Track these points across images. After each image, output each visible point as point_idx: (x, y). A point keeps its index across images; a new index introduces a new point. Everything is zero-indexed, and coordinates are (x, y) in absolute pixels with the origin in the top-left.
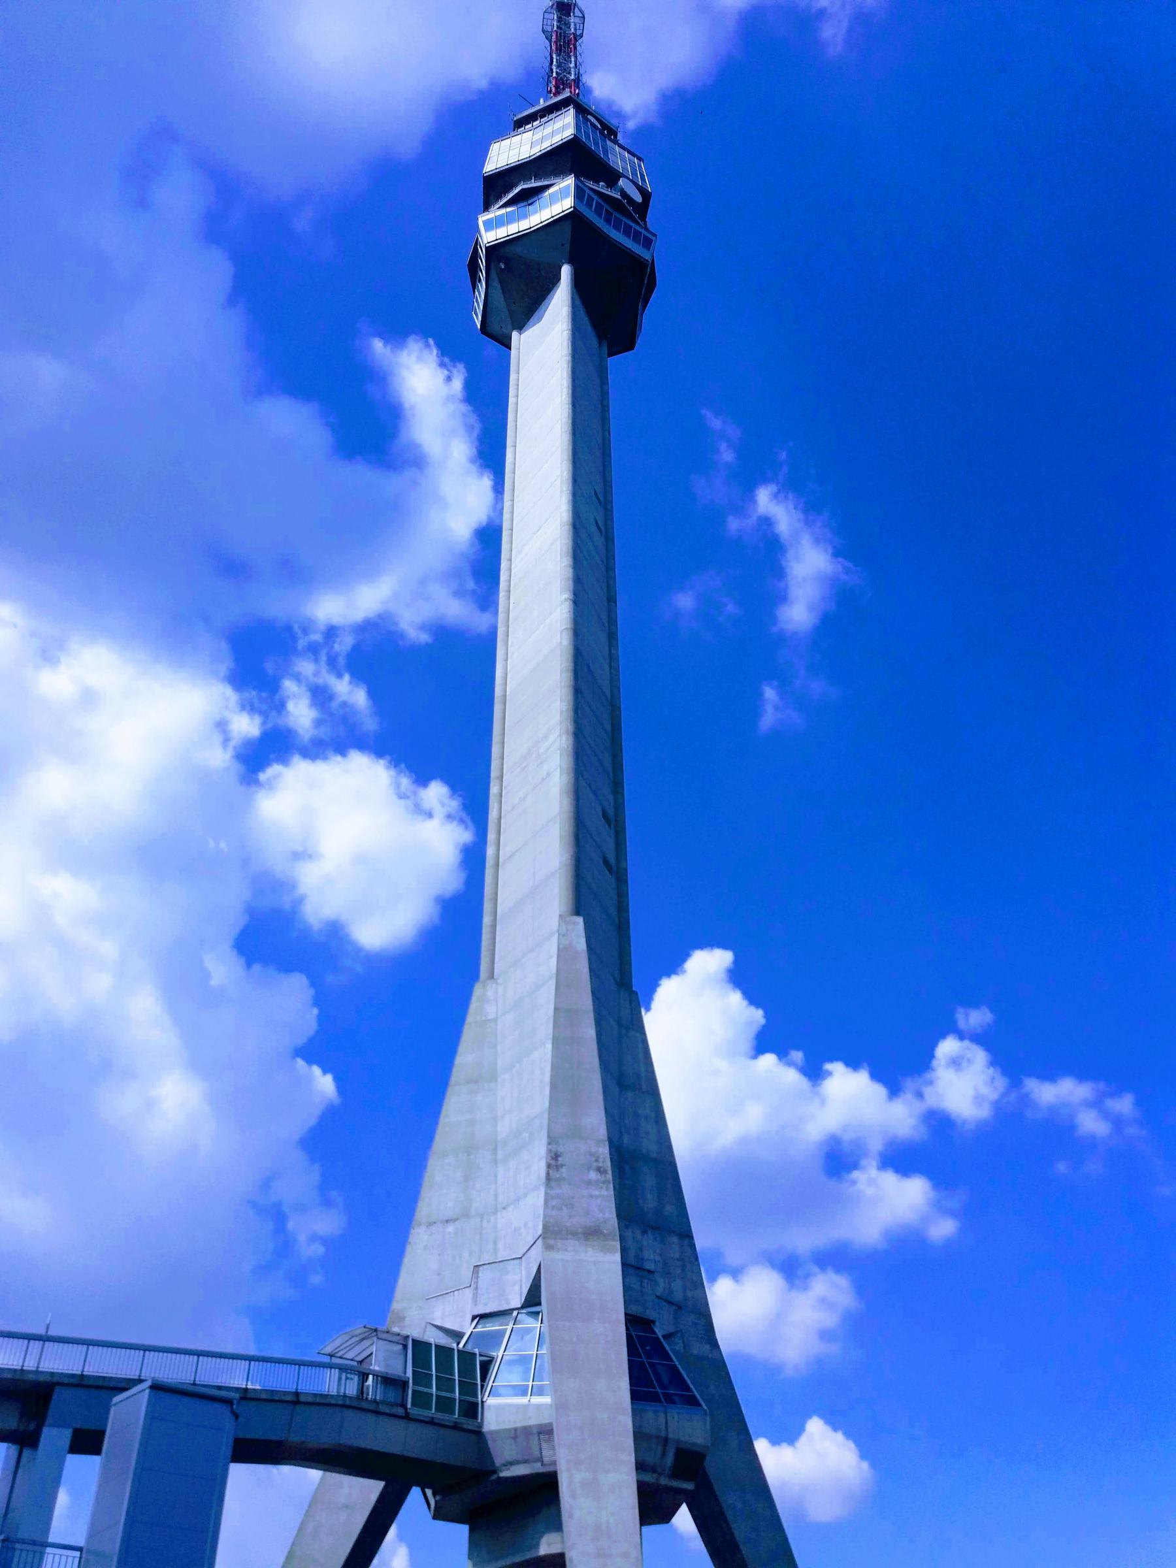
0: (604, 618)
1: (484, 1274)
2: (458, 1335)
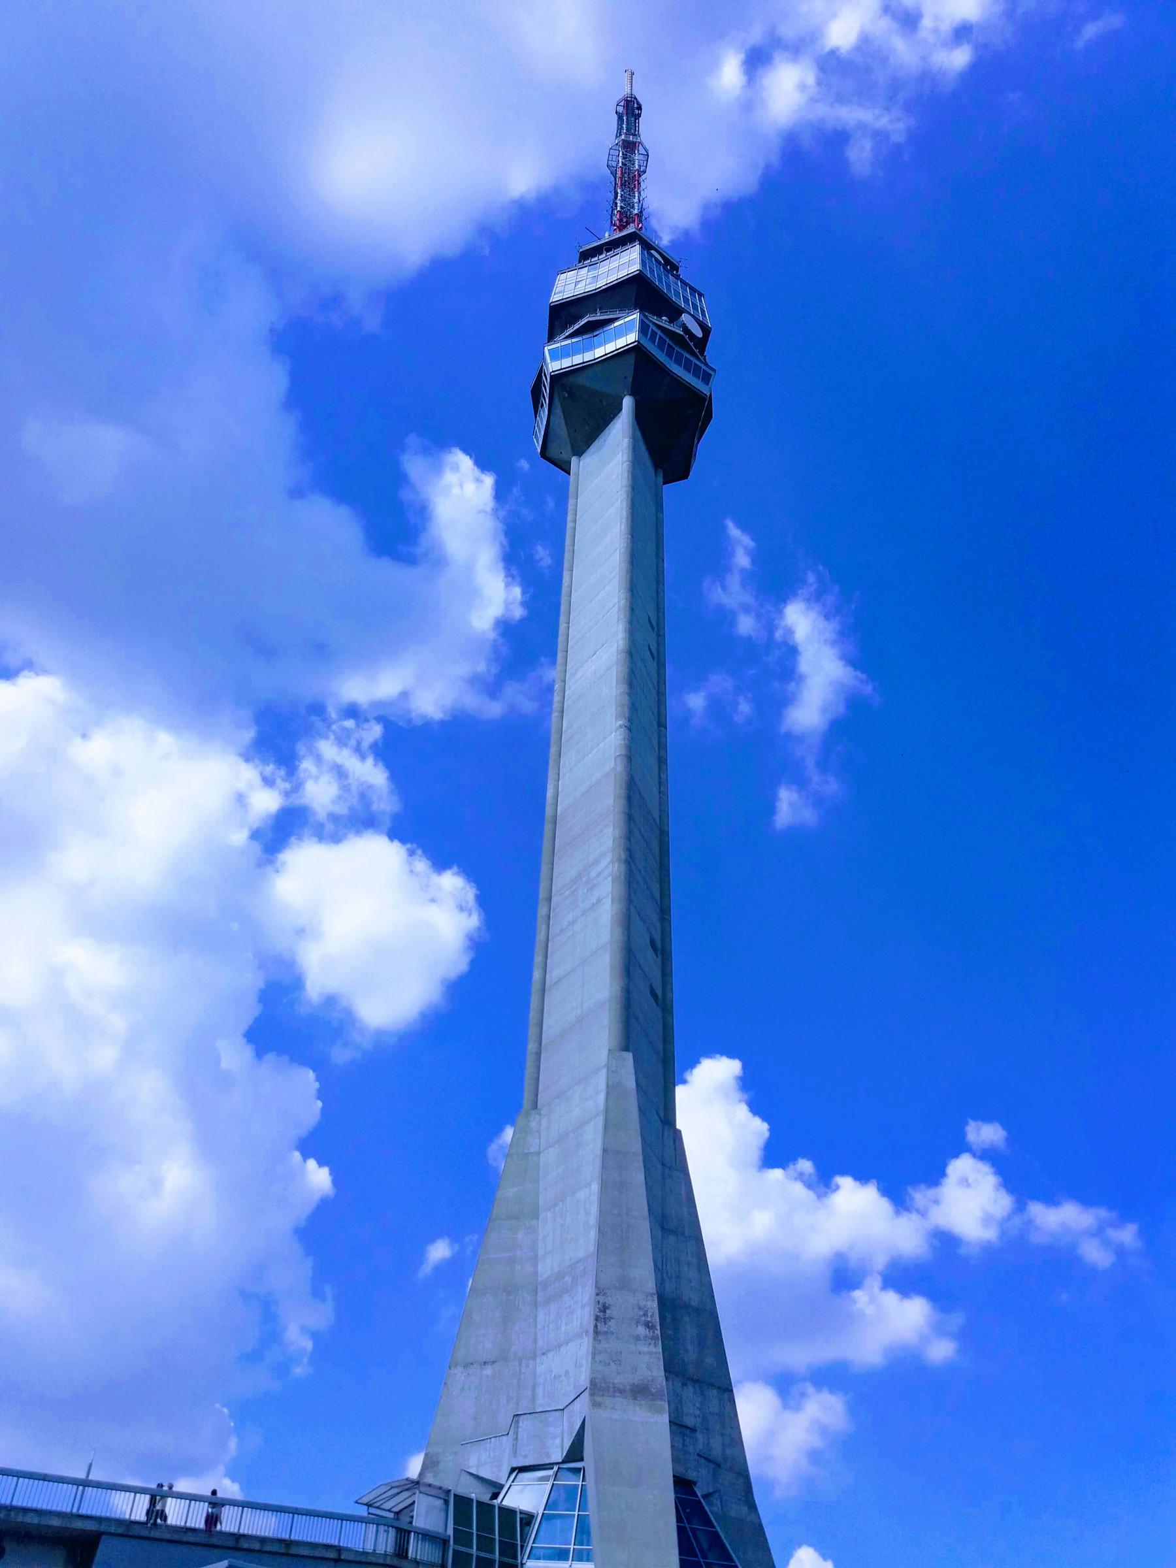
1: (525, 1424)
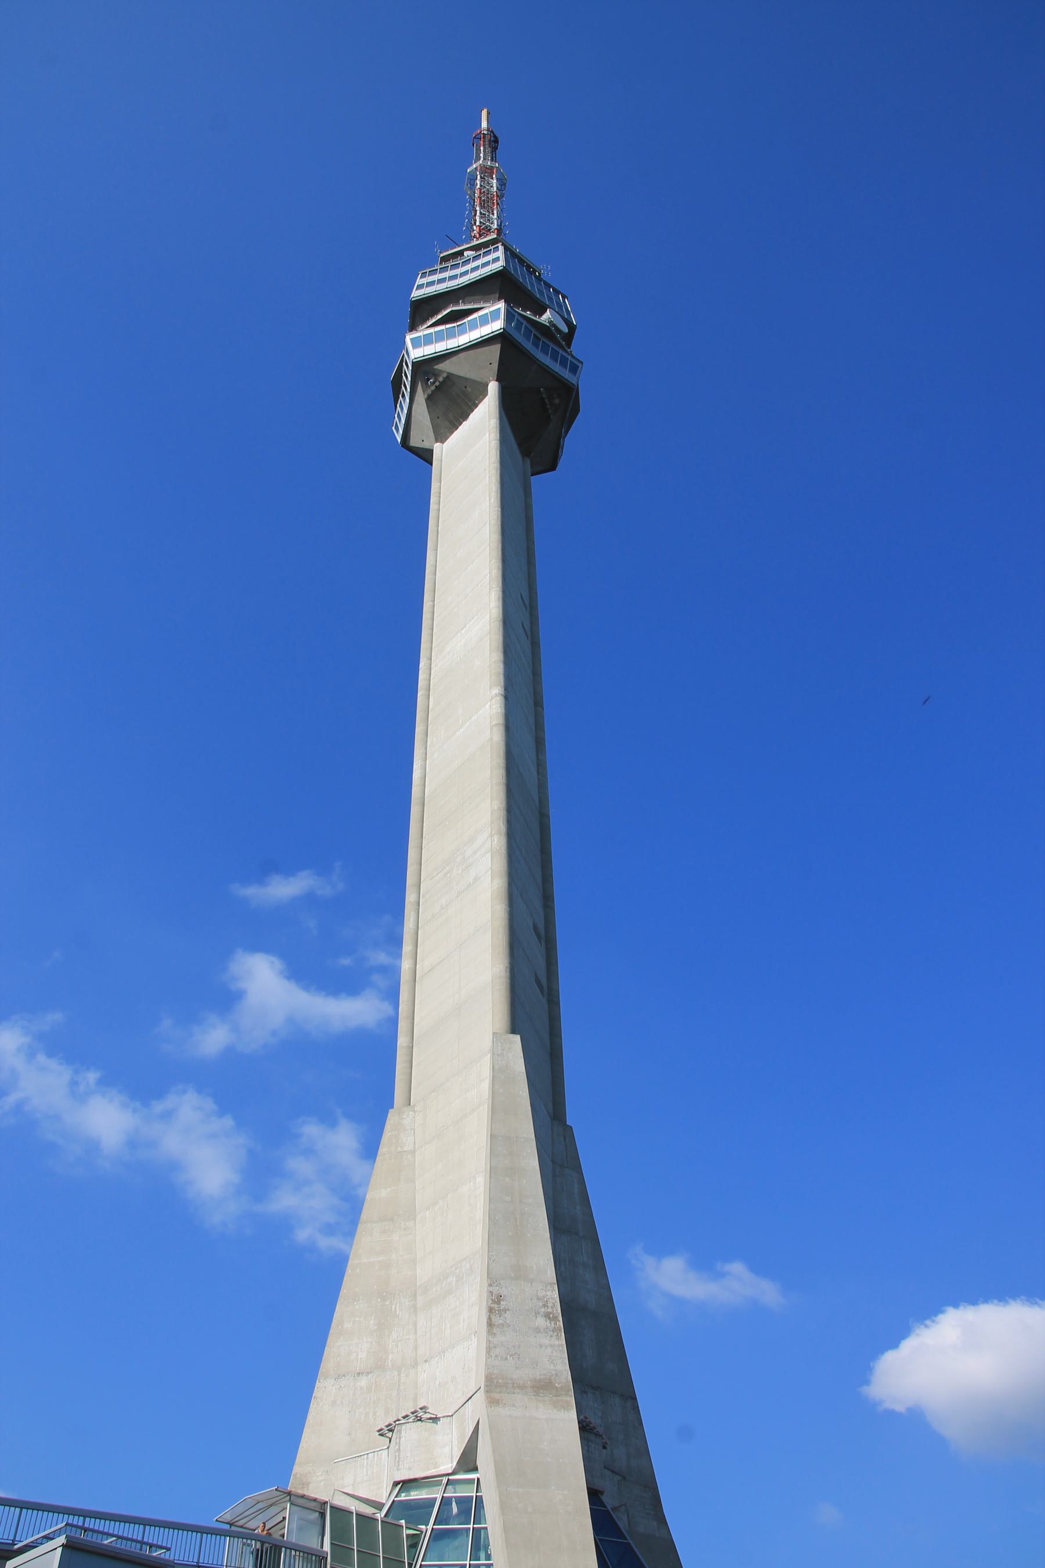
0: (532, 720)
2: (379, 1506)
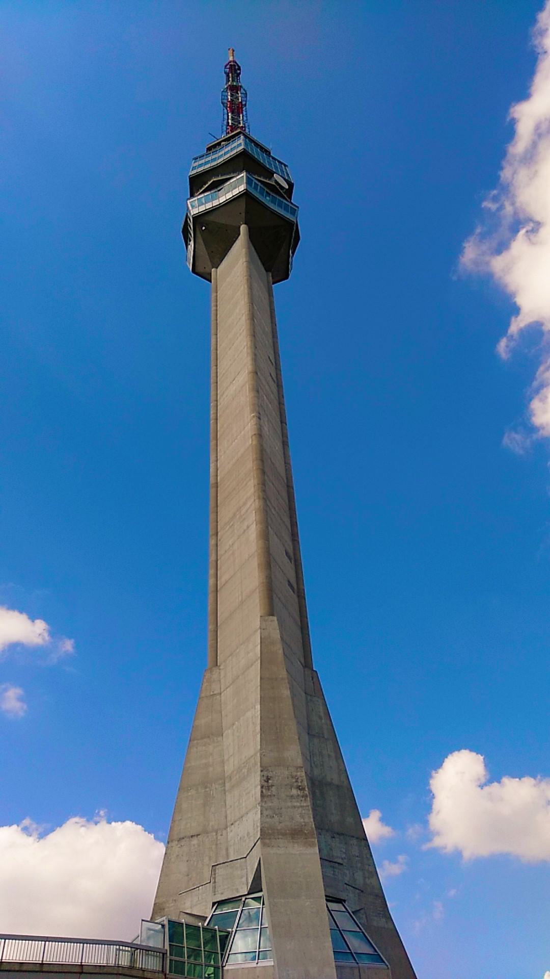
0: (279, 432)
1: (220, 871)
